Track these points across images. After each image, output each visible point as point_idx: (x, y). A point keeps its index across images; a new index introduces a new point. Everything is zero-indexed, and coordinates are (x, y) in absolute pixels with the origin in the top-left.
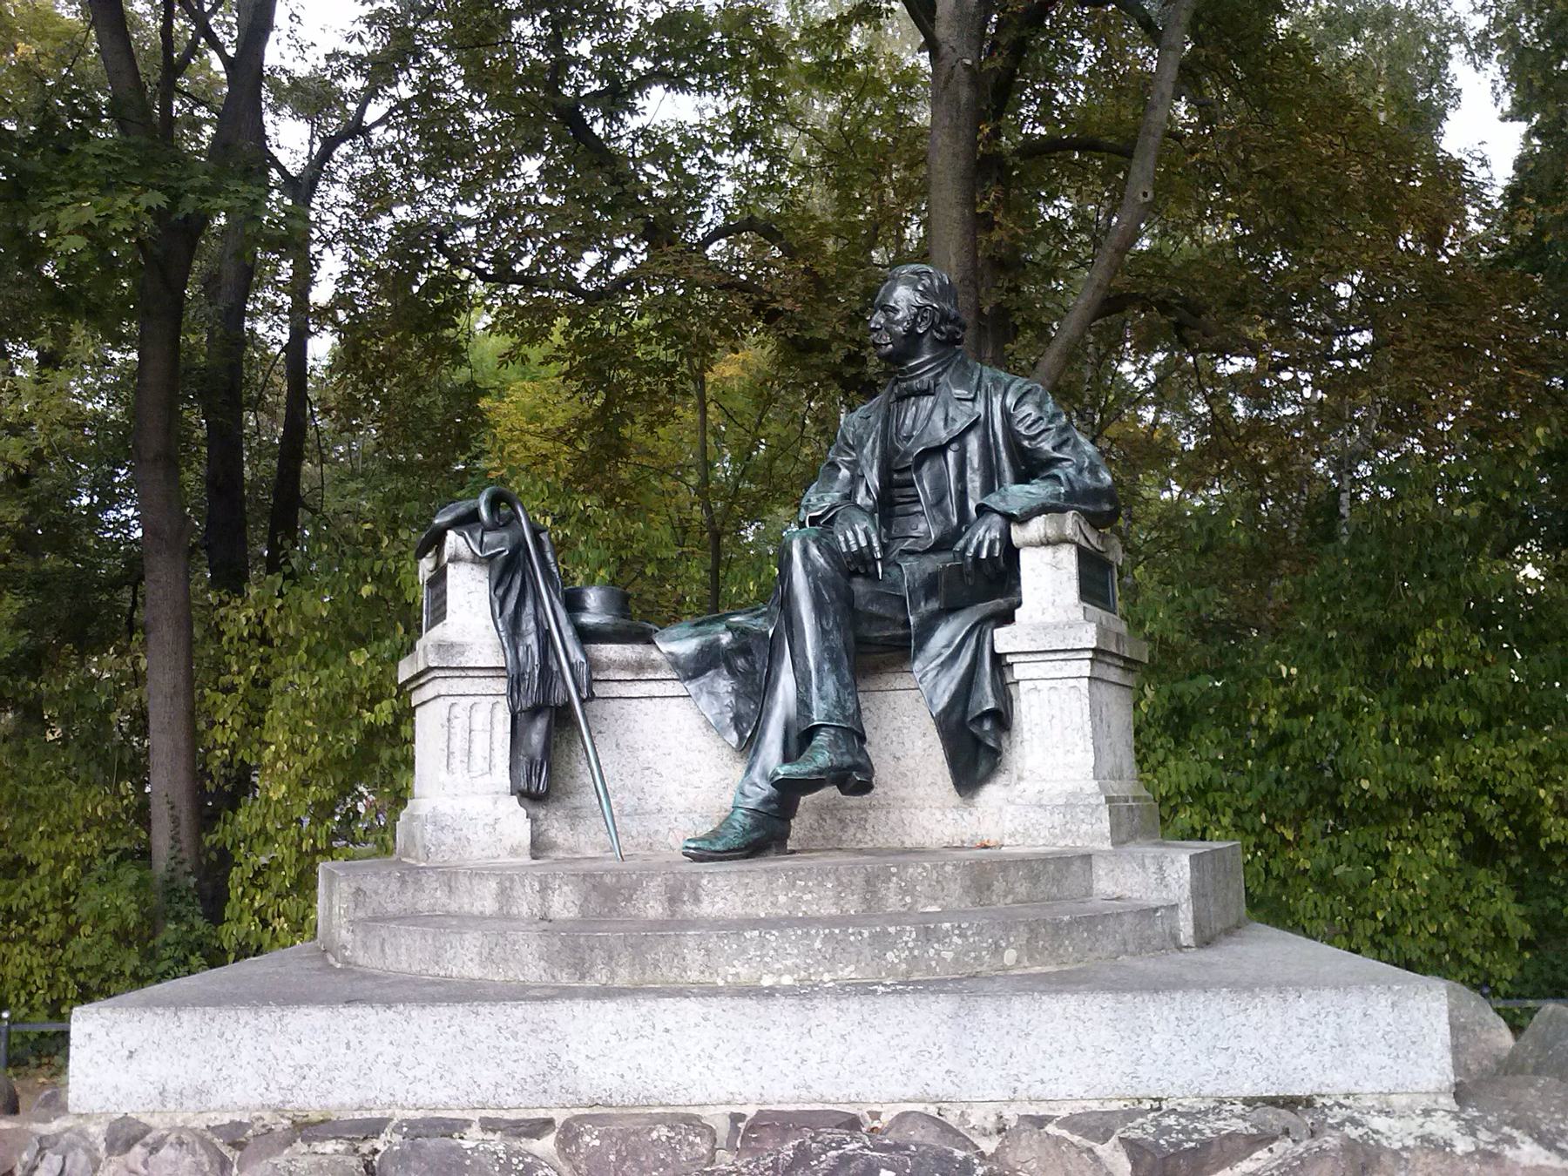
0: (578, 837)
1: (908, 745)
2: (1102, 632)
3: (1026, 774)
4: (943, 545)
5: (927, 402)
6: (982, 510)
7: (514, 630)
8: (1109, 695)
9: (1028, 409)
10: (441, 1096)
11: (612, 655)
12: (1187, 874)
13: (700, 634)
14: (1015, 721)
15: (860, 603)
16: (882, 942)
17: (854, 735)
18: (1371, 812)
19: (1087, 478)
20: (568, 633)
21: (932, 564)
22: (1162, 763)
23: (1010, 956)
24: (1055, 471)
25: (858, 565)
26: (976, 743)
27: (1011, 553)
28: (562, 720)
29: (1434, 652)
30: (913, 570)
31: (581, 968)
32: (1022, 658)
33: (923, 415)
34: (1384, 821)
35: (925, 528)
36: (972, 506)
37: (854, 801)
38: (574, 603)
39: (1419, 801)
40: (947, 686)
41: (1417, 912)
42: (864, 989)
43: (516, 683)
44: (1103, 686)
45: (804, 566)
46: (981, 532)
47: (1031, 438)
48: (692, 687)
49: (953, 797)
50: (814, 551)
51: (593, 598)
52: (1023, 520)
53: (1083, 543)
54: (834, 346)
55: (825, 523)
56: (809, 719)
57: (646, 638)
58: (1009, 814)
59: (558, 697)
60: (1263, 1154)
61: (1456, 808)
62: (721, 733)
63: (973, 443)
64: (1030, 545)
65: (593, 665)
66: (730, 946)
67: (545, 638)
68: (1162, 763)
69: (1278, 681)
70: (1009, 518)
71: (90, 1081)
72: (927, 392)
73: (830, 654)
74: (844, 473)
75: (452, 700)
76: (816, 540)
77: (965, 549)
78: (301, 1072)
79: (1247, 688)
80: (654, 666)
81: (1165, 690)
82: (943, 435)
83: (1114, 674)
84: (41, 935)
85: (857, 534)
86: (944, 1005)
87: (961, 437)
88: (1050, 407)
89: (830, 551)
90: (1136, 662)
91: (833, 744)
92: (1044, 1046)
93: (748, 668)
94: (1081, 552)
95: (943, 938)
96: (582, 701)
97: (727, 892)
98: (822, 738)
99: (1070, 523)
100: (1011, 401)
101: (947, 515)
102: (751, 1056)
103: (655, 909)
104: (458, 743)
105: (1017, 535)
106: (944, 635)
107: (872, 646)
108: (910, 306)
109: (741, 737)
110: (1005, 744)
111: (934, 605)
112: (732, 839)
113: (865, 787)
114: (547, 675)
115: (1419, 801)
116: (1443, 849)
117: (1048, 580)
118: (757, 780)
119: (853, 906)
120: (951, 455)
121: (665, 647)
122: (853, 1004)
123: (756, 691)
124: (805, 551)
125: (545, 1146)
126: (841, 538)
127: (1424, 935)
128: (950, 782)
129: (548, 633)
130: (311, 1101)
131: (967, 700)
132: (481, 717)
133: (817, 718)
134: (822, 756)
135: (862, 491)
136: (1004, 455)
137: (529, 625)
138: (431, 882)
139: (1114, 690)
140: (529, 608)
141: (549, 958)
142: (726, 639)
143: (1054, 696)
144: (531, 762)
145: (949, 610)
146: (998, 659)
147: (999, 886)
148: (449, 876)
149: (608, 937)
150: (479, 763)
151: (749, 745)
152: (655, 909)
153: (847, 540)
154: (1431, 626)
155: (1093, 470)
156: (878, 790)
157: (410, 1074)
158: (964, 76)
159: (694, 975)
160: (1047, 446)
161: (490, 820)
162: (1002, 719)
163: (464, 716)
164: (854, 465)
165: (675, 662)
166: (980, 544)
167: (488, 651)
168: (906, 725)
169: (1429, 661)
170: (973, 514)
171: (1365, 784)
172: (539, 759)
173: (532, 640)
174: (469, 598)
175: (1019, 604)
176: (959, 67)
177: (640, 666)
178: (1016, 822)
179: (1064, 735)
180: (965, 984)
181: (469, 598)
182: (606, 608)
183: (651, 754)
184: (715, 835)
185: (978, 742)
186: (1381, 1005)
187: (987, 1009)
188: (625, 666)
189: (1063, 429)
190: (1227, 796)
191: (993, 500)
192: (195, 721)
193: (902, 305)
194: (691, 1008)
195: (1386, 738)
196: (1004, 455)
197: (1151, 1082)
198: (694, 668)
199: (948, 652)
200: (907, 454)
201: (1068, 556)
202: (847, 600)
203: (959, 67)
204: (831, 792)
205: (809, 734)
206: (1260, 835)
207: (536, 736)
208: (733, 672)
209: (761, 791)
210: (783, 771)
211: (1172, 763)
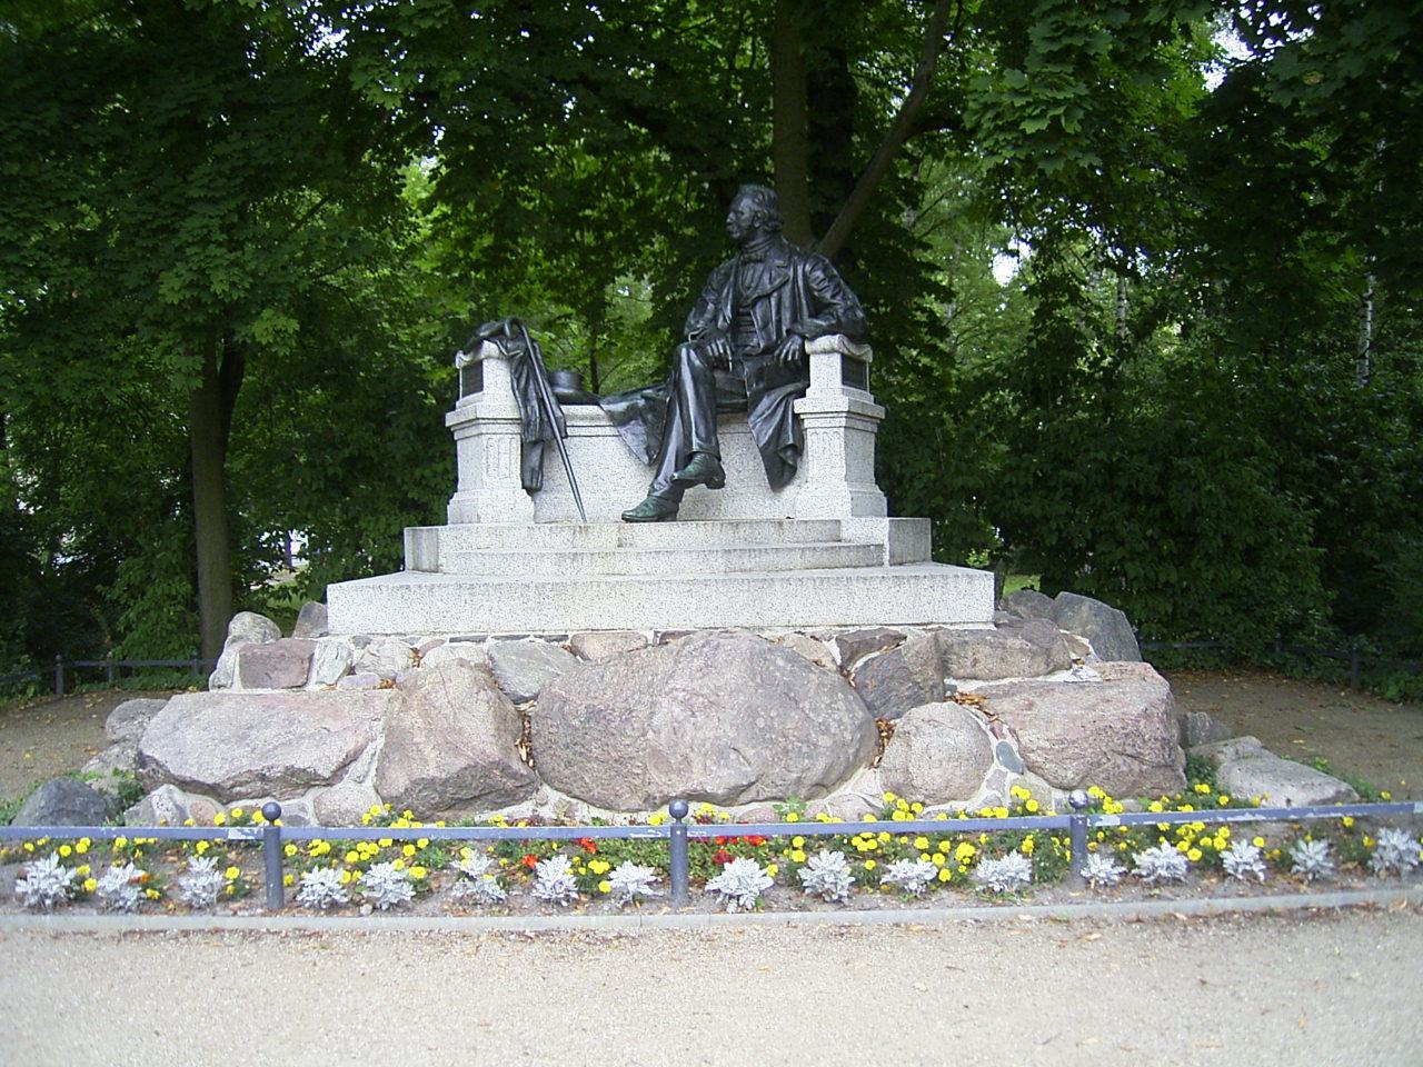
5: (760, 267)
7: (526, 400)
12: (887, 530)
20: (553, 400)
25: (719, 363)
26: (782, 463)
27: (805, 358)
33: (757, 275)
35: (758, 342)
36: (784, 329)
38: (553, 383)
44: (853, 432)
48: (622, 430)
51: (563, 377)
53: (846, 352)
63: (787, 290)
67: (541, 401)
72: (761, 261)
77: (780, 355)
83: (859, 425)
85: (718, 347)
87: (779, 288)
92: (804, 601)
94: (844, 357)
95: (895, 374)
98: (698, 458)
100: (808, 268)
101: (769, 335)
105: (808, 347)
107: (725, 407)
109: (650, 458)
110: (799, 463)
113: (721, 485)
117: (825, 370)
121: (605, 407)
129: (543, 399)
131: (779, 438)
132: (504, 446)
133: (695, 448)
135: (721, 319)
136: (804, 302)
140: (531, 387)
144: (533, 470)
145: (769, 389)
146: (796, 416)
150: (503, 471)
151: (656, 461)
156: (727, 489)
162: (798, 449)
164: (716, 303)
166: (787, 353)
168: (740, 455)
170: (785, 334)
173: (535, 403)
175: (809, 386)
181: (497, 376)
185: (784, 462)
193: (746, 211)
196: (804, 302)
198: (619, 420)
199: (767, 413)
200: (748, 298)
201: (836, 360)
205: (690, 457)
207: (535, 458)
208: (645, 422)
209: (663, 487)
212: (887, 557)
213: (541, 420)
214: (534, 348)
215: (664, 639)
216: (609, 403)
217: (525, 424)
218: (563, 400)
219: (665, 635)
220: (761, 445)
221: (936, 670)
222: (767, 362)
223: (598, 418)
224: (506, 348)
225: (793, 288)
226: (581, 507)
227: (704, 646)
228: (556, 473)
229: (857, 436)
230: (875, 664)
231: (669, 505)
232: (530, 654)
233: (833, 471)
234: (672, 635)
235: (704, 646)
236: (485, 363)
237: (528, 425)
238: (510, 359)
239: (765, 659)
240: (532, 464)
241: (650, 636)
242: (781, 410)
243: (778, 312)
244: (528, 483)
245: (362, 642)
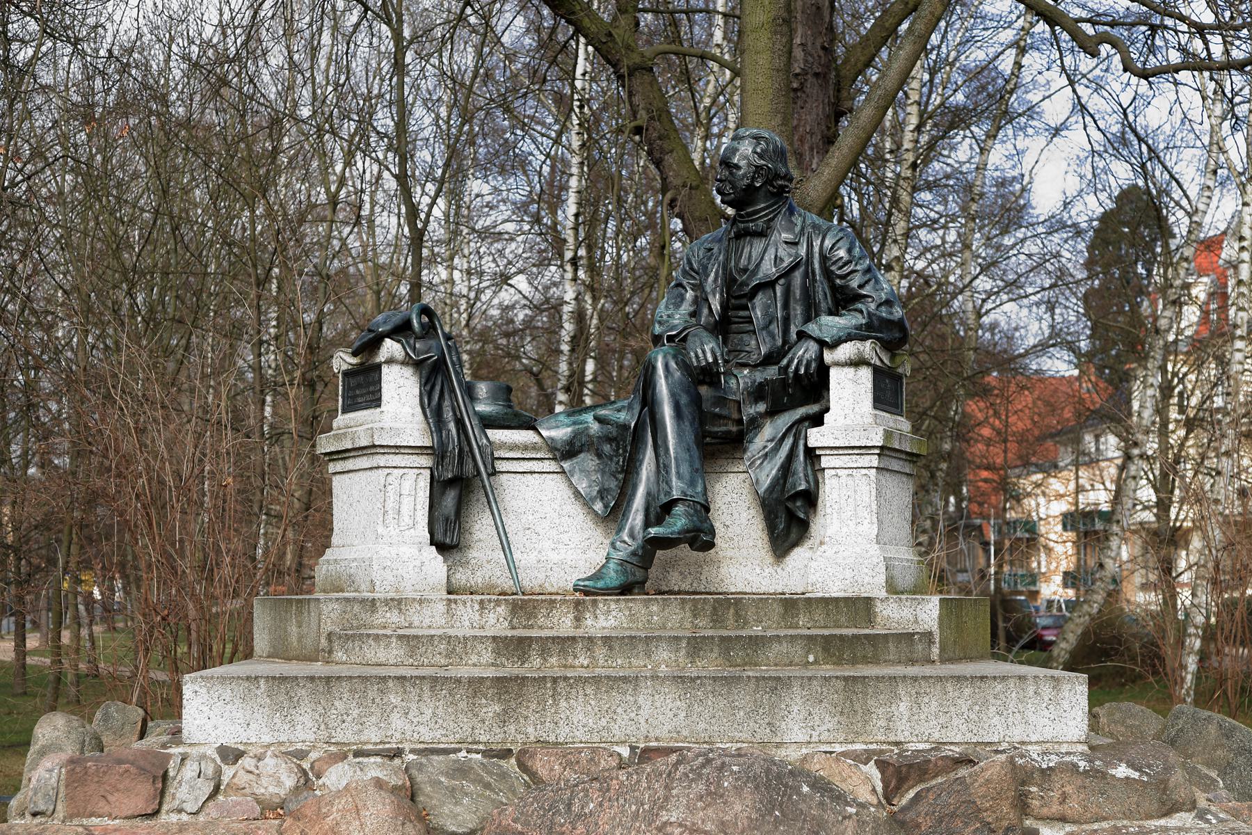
1: (736, 515)
2: (888, 434)
3: (827, 539)
4: (770, 359)
8: (891, 482)
11: (503, 439)
12: (936, 613)
13: (574, 423)
14: (820, 500)
15: (706, 406)
20: (475, 422)
24: (860, 306)
25: (707, 375)
26: (790, 515)
30: (744, 378)
32: (828, 452)
37: (712, 551)
40: (768, 473)
45: (666, 377)
46: (801, 353)
47: (843, 277)
48: (566, 465)
49: (769, 558)
50: (673, 364)
52: (834, 345)
53: (878, 363)
56: (668, 493)
64: (837, 364)
67: (460, 423)
70: (822, 344)
71: (197, 722)
72: (762, 234)
75: (388, 471)
76: (675, 357)
77: (788, 365)
83: (895, 465)
85: (706, 350)
89: (685, 366)
90: (918, 456)
93: (621, 451)
94: (878, 373)
96: (489, 475)
97: (609, 618)
98: (679, 509)
99: (867, 348)
102: (641, 712)
104: (390, 504)
105: (828, 357)
106: (769, 431)
107: (718, 443)
108: (749, 165)
111: (761, 407)
113: (710, 545)
118: (626, 539)
120: (779, 289)
124: (666, 367)
126: (692, 354)
128: (767, 546)
132: (407, 485)
134: (679, 521)
135: (705, 311)
137: (448, 414)
139: (897, 478)
140: (447, 403)
143: (850, 482)
145: (772, 413)
146: (812, 455)
150: (406, 520)
151: (614, 514)
153: (697, 356)
157: (415, 720)
160: (854, 284)
161: (418, 563)
162: (810, 499)
163: (396, 483)
164: (699, 287)
167: (417, 434)
172: (453, 518)
173: (452, 426)
175: (827, 410)
178: (818, 575)
182: (493, 398)
183: (531, 517)
184: (597, 576)
185: (791, 515)
189: (868, 270)
191: (812, 328)
198: (566, 452)
201: (866, 374)
202: (697, 400)
204: (684, 550)
205: (668, 507)
209: (628, 543)
212: (936, 650)
213: (461, 450)
214: (448, 347)
215: (646, 755)
216: (548, 429)
217: (438, 452)
218: (488, 422)
219: (646, 750)
220: (761, 491)
221: (1014, 806)
222: (772, 372)
223: (534, 447)
224: (414, 349)
225: (806, 275)
226: (679, 593)
227: (703, 766)
228: (481, 528)
229: (889, 480)
230: (931, 796)
231: (639, 574)
232: (462, 771)
233: (860, 528)
234: (657, 750)
235: (703, 766)
236: (385, 369)
237: (443, 458)
238: (417, 365)
239: (786, 786)
240: (446, 512)
241: (625, 752)
242: (789, 442)
243: (786, 306)
244: (439, 537)
245: (231, 755)
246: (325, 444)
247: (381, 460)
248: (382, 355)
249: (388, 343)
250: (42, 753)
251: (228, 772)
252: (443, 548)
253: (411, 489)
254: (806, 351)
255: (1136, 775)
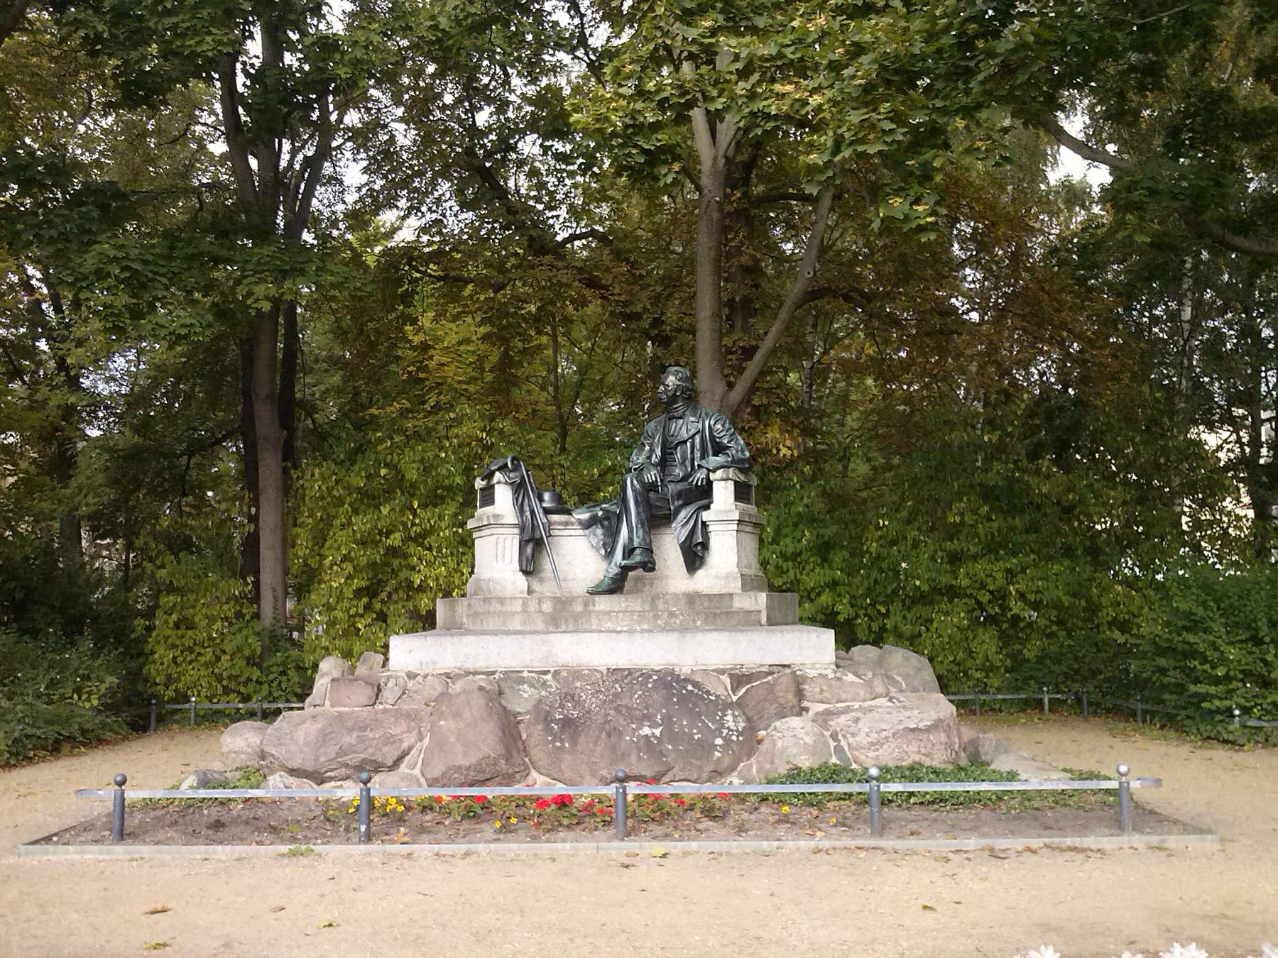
0: (546, 588)
4: (685, 479)
6: (699, 466)
9: (719, 426)
10: (513, 664)
16: (656, 617)
17: (649, 550)
18: (922, 599)
19: (740, 455)
20: (541, 511)
21: (680, 486)
22: (812, 570)
23: (699, 623)
25: (652, 487)
26: (695, 555)
27: (710, 483)
28: (538, 544)
29: (962, 514)
30: (672, 489)
31: (557, 625)
34: (932, 602)
35: (679, 472)
39: (953, 592)
40: (685, 533)
41: (944, 650)
42: (650, 631)
43: (522, 529)
48: (587, 532)
51: (547, 496)
52: (714, 471)
54: (645, 316)
55: (640, 470)
57: (569, 512)
58: (706, 580)
59: (537, 535)
60: (770, 678)
61: (970, 596)
62: (598, 550)
63: (697, 438)
65: (550, 523)
66: (606, 617)
67: (532, 512)
68: (812, 570)
69: (878, 528)
70: (709, 470)
73: (641, 522)
74: (647, 448)
78: (467, 656)
79: (863, 531)
80: (572, 524)
81: (815, 532)
82: (686, 436)
83: (748, 529)
84: (202, 659)
85: (652, 475)
86: (675, 635)
88: (727, 426)
89: (641, 482)
91: (642, 554)
93: (610, 524)
94: (736, 483)
97: (603, 603)
98: (638, 551)
100: (712, 422)
103: (579, 608)
104: (500, 552)
105: (712, 476)
106: (683, 514)
107: (657, 518)
112: (604, 587)
113: (653, 569)
114: (534, 527)
115: (953, 592)
116: (960, 617)
117: (723, 493)
119: (647, 607)
122: (646, 635)
123: (612, 534)
125: (549, 677)
127: (946, 662)
130: (470, 665)
132: (508, 543)
137: (526, 508)
138: (494, 602)
141: (546, 623)
142: (600, 513)
145: (686, 504)
146: (704, 523)
147: (698, 602)
148: (502, 600)
149: (563, 615)
150: (507, 559)
151: (609, 555)
152: (579, 608)
154: (961, 500)
155: (742, 451)
158: (714, 206)
159: (594, 627)
162: (705, 545)
164: (651, 445)
165: (580, 522)
169: (958, 519)
171: (918, 583)
173: (528, 514)
174: (503, 495)
176: (713, 203)
177: (567, 524)
179: (728, 552)
180: (684, 629)
184: (598, 586)
185: (695, 554)
186: (805, 635)
187: (689, 636)
188: (561, 523)
190: (847, 588)
191: (703, 463)
192: (287, 543)
194: (595, 635)
195: (933, 558)
197: (740, 660)
198: (587, 525)
201: (731, 485)
203: (713, 203)
206: (866, 609)
207: (529, 550)
209: (614, 570)
210: (624, 563)
211: (817, 571)
246: (471, 524)
247: (494, 531)
248: (495, 480)
249: (497, 474)
250: (322, 676)
251: (410, 684)
252: (526, 573)
253: (510, 543)
254: (701, 475)
255: (857, 680)
